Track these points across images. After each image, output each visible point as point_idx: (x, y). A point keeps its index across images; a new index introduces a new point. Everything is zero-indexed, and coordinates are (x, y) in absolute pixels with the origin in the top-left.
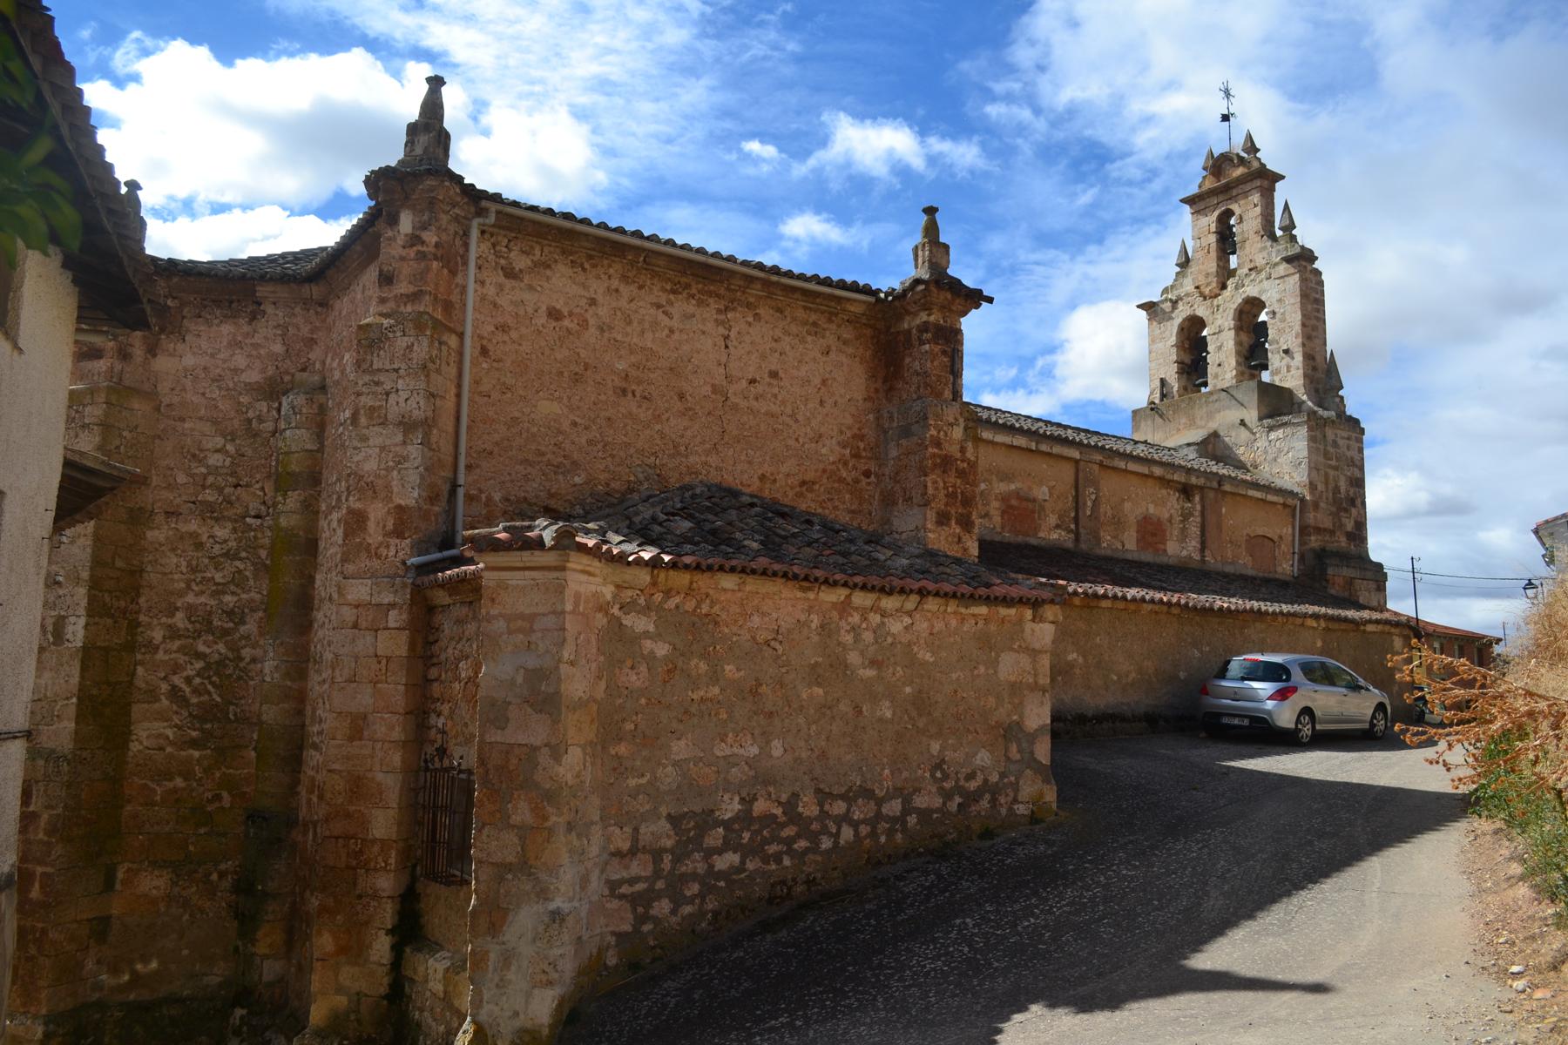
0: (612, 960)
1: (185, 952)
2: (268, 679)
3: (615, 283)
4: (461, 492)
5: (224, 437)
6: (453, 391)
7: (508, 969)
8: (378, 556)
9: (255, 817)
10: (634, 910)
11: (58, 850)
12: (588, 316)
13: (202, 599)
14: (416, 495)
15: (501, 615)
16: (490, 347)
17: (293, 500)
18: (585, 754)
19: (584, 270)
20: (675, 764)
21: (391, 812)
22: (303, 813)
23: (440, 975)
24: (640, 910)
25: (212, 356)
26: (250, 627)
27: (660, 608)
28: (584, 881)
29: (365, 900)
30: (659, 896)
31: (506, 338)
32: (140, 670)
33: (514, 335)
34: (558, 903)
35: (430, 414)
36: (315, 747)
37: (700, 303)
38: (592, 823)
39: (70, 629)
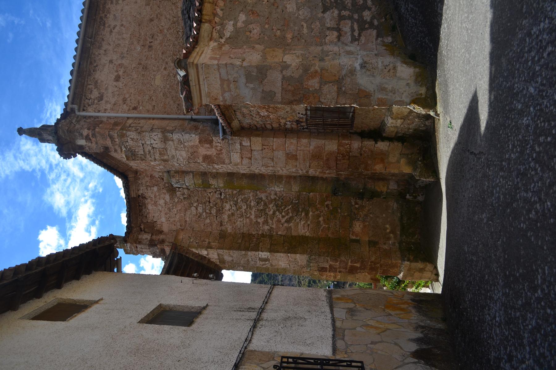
0: (389, 39)
1: (384, 215)
2: (282, 189)
3: (102, 52)
4: (195, 117)
5: (191, 207)
6: (151, 121)
7: (386, 88)
8: (221, 150)
9: (335, 193)
10: (367, 29)
11: (343, 258)
12: (117, 64)
13: (253, 213)
14: (194, 135)
15: (222, 95)
16: (133, 106)
17: (212, 182)
18: (288, 54)
19: (97, 66)
20: (298, 9)
21: (327, 143)
22: (334, 176)
23: (394, 121)
24: (367, 26)
25: (161, 212)
26: (263, 196)
27: (222, 19)
28: (349, 53)
29: (363, 152)
30: (361, 17)
31: (129, 99)
32: (279, 233)
33: (127, 96)
34: (357, 66)
35: (159, 130)
36: (307, 172)
37: (109, 12)
38: (322, 50)
39: (263, 257)
